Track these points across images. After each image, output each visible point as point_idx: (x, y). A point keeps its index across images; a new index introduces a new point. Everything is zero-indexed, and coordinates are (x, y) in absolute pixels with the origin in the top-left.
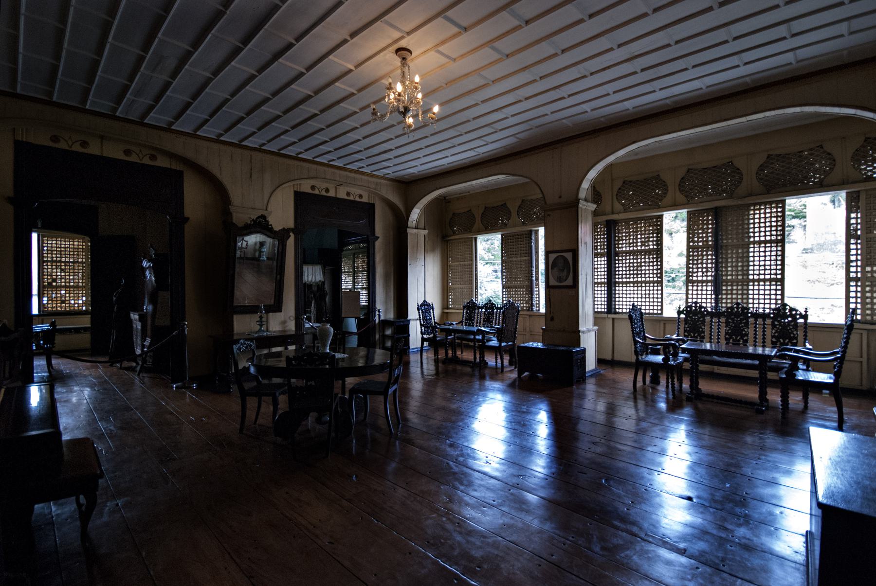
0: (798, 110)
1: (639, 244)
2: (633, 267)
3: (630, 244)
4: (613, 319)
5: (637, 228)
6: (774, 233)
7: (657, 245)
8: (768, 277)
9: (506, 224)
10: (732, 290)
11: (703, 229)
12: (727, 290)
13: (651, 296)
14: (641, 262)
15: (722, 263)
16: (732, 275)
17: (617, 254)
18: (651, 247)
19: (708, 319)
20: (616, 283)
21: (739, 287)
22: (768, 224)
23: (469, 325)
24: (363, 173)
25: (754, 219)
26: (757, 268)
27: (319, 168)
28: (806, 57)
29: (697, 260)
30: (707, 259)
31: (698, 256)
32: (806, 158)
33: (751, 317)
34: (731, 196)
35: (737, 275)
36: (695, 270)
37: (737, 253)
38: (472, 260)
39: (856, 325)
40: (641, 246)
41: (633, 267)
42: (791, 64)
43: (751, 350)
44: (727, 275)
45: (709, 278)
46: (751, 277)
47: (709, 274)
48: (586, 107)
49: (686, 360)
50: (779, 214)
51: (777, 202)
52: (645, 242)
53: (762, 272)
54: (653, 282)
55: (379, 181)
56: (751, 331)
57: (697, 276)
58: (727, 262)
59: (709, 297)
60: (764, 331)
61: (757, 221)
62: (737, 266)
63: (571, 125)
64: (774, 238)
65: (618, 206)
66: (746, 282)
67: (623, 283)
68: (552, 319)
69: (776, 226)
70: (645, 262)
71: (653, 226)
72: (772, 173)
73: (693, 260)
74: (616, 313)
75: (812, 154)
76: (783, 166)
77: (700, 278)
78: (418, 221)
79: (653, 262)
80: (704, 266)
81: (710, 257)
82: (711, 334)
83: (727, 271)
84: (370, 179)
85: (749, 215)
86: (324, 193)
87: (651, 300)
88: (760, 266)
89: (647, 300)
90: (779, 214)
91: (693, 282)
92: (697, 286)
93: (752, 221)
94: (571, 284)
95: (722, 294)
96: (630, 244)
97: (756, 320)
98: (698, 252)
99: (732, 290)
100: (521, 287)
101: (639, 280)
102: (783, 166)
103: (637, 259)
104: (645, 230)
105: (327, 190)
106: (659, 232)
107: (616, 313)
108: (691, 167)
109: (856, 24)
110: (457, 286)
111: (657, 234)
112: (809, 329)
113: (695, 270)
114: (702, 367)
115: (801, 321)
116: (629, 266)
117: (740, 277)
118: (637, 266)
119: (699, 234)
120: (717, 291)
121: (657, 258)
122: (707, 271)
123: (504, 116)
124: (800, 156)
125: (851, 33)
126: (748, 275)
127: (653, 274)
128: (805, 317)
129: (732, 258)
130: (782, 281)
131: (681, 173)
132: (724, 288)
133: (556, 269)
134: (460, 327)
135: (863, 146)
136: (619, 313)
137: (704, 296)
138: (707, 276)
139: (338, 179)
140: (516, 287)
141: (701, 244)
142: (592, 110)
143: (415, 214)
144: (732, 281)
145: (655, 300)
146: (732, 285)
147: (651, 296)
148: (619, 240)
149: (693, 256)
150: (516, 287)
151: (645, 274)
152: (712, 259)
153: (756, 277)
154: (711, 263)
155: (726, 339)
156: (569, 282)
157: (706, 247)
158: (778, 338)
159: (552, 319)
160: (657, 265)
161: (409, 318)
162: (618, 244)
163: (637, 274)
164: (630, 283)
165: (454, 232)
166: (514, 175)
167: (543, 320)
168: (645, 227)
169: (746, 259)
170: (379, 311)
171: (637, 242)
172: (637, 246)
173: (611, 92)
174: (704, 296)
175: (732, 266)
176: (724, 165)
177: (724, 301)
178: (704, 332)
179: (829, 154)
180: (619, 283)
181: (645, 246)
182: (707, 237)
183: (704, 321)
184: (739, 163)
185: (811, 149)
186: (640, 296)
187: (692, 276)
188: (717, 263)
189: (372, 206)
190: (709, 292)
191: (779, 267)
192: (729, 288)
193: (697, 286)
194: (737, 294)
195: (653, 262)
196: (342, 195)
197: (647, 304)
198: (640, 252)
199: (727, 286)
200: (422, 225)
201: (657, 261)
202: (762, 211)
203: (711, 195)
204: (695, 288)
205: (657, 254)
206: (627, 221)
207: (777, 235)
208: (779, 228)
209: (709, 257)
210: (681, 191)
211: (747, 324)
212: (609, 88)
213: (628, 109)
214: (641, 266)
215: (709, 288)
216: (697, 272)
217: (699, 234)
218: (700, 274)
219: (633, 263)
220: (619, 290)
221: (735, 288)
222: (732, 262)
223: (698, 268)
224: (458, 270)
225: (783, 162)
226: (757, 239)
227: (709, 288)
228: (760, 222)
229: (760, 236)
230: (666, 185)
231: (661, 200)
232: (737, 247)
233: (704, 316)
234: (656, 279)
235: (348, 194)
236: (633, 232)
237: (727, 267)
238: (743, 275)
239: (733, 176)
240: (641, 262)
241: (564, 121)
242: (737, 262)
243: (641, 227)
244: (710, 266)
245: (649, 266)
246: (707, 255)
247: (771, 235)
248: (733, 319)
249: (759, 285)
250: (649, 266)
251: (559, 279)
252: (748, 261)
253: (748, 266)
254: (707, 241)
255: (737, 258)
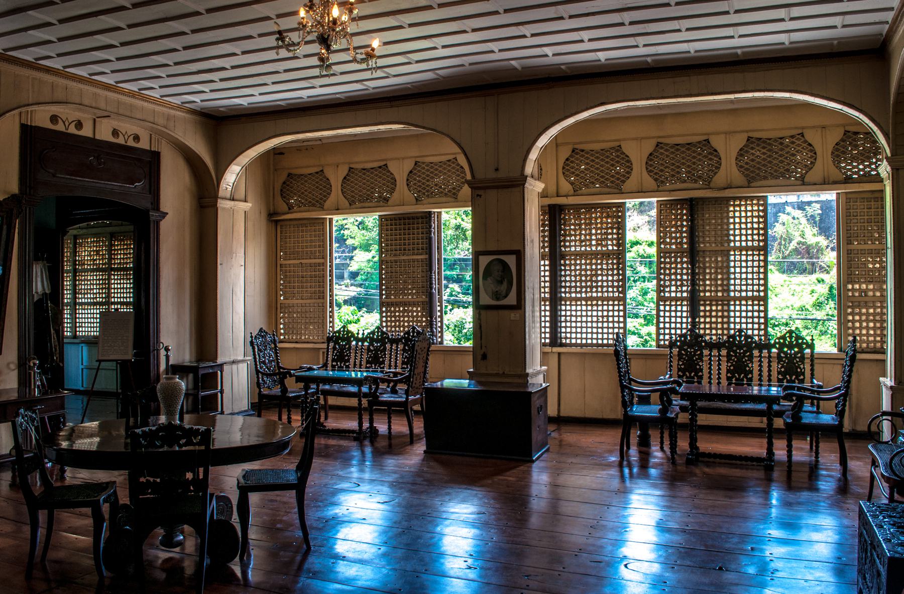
0: (787, 95)
1: (594, 243)
2: (586, 276)
3: (581, 241)
4: (559, 354)
5: (591, 218)
6: (756, 237)
7: (618, 245)
8: (750, 294)
9: (386, 200)
10: (711, 311)
11: (676, 226)
12: (705, 311)
13: (611, 319)
14: (596, 270)
15: (699, 274)
16: (710, 291)
17: (563, 256)
18: (610, 248)
19: (756, 353)
20: (561, 299)
21: (719, 308)
22: (749, 225)
23: (340, 369)
24: (48, 70)
25: (734, 217)
26: (738, 282)
27: (71, 84)
28: (801, 39)
29: (670, 269)
30: (682, 269)
31: (670, 263)
32: (787, 146)
33: (755, 348)
34: (708, 186)
35: (717, 291)
36: (667, 283)
37: (716, 261)
38: (324, 257)
39: (859, 356)
40: (597, 245)
41: (586, 276)
42: (783, 43)
43: (755, 390)
44: (705, 291)
45: (685, 295)
46: (732, 294)
47: (685, 288)
48: (548, 51)
49: (683, 409)
50: (761, 214)
51: (759, 198)
52: (602, 240)
53: (744, 288)
54: (613, 299)
55: (172, 112)
56: (756, 366)
57: (670, 292)
58: (705, 274)
59: (684, 320)
60: (719, 364)
61: (737, 220)
62: (716, 279)
63: (519, 67)
64: (756, 244)
65: (566, 187)
66: (726, 301)
67: (571, 299)
68: (484, 357)
69: (758, 229)
70: (602, 269)
71: (612, 217)
72: (753, 160)
73: (665, 269)
74: (562, 345)
75: (793, 143)
76: (764, 154)
77: (673, 295)
78: (235, 186)
79: (612, 270)
80: (679, 277)
81: (685, 266)
82: (710, 373)
83: (705, 285)
84: (158, 108)
85: (728, 211)
86: (72, 130)
87: (611, 325)
88: (741, 279)
89: (605, 325)
90: (761, 214)
91: (665, 299)
92: (671, 305)
93: (731, 220)
94: (514, 303)
95: (700, 317)
96: (581, 241)
97: (761, 352)
98: (670, 258)
99: (711, 311)
100: (414, 304)
101: (594, 295)
102: (764, 154)
103: (591, 264)
104: (601, 223)
105: (79, 125)
106: (621, 227)
107: (562, 345)
108: (660, 140)
109: (850, 19)
110: (295, 302)
111: (618, 229)
112: (816, 361)
113: (667, 283)
114: (703, 419)
115: (808, 351)
116: (580, 275)
117: (720, 294)
118: (592, 276)
119: (671, 233)
120: (694, 313)
121: (618, 264)
122: (682, 285)
123: (432, 46)
124: (781, 144)
125: (844, 26)
126: (728, 291)
127: (613, 287)
128: (811, 346)
129: (710, 268)
130: (765, 299)
131: (649, 147)
132: (702, 308)
133: (489, 280)
134: (322, 373)
135: (842, 140)
136: (565, 345)
137: (679, 320)
138: (682, 292)
139: (102, 105)
140: (405, 304)
141: (674, 247)
142: (554, 55)
143: (232, 176)
144: (711, 299)
145: (616, 325)
146: (711, 305)
147: (611, 319)
148: (565, 235)
149: (665, 263)
150: (405, 304)
151: (602, 287)
152: (687, 269)
153: (737, 294)
154: (687, 274)
155: (728, 379)
156: (512, 299)
157: (680, 252)
158: (784, 374)
159: (484, 357)
160: (618, 274)
161: (220, 360)
162: (565, 241)
163: (591, 287)
164: (581, 299)
165: (290, 207)
166: (424, 128)
167: (469, 359)
168: (601, 218)
169: (725, 269)
170: (167, 349)
171: (591, 240)
172: (591, 245)
173: (586, 38)
174: (679, 320)
175: (710, 279)
176: (699, 142)
177: (702, 326)
178: (701, 370)
179: (810, 145)
180: (566, 299)
181: (601, 245)
182: (682, 237)
183: (701, 355)
184: (717, 142)
185: (792, 137)
186: (595, 319)
187: (664, 291)
188: (693, 274)
189: (155, 157)
190: (685, 314)
191: (762, 282)
192: (708, 308)
193: (671, 305)
194: (717, 317)
195: (612, 270)
196: (104, 134)
197: (605, 330)
198: (595, 255)
199: (705, 305)
200: (241, 194)
201: (618, 269)
202: (743, 208)
203: (685, 181)
204: (667, 308)
205: (618, 259)
206: (577, 208)
207: (759, 241)
208: (761, 232)
209: (683, 265)
210: (649, 172)
211: (751, 357)
212: (585, 35)
213: (600, 60)
214: (597, 275)
215: (685, 308)
216: (670, 286)
217: (671, 233)
218: (673, 288)
219: (586, 270)
220: (566, 310)
221: (714, 308)
222: (710, 273)
223: (670, 280)
224: (297, 270)
225: (764, 148)
226: (738, 244)
227: (685, 308)
228: (741, 220)
229: (741, 241)
230: (629, 161)
231: (624, 182)
232: (716, 253)
233: (750, 349)
234: (616, 294)
235: (115, 133)
236: (586, 224)
237: (704, 280)
238: (723, 291)
239: (711, 159)
240: (596, 270)
241: (513, 62)
242: (716, 273)
243: (596, 218)
244: (685, 277)
245: (607, 275)
246: (682, 263)
247: (753, 240)
248: (735, 352)
249: (740, 305)
250: (607, 275)
251: (497, 296)
252: (729, 273)
253: (729, 279)
254: (681, 243)
255: (716, 268)
